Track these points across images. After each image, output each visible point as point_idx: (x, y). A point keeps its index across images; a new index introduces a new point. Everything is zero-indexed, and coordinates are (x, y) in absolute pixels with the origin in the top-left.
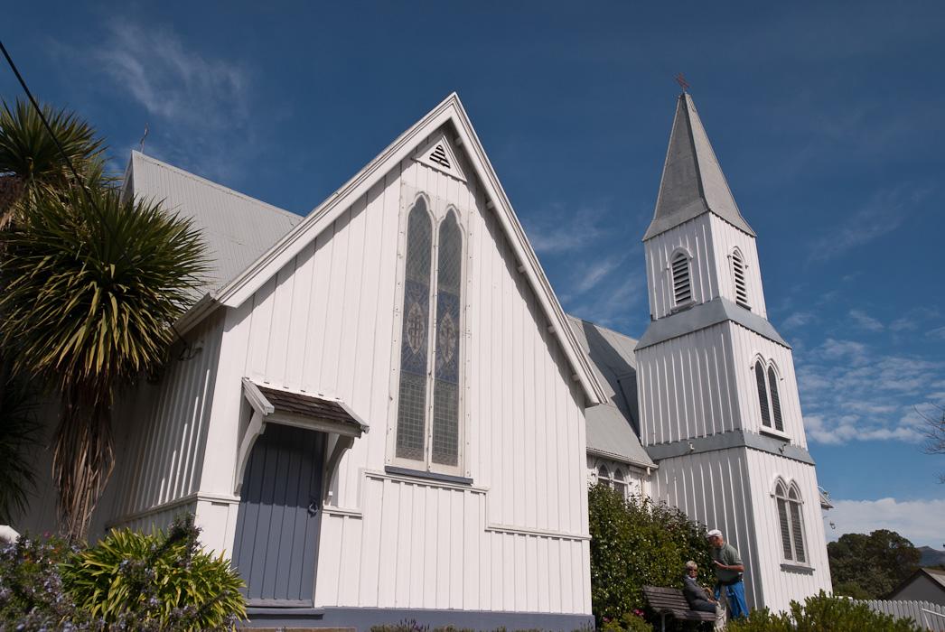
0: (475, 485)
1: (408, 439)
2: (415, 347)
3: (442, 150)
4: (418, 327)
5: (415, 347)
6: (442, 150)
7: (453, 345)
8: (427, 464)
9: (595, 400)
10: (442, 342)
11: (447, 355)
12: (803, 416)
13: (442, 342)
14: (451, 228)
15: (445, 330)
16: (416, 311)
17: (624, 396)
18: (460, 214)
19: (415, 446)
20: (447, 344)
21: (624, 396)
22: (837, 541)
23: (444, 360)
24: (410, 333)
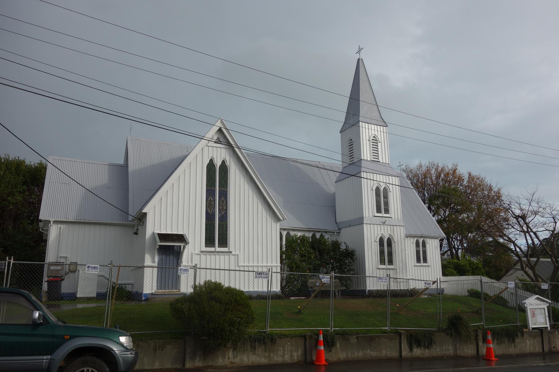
0: (233, 253)
1: (209, 241)
2: (210, 212)
3: (219, 138)
4: (211, 204)
5: (210, 212)
6: (219, 138)
7: (225, 208)
8: (422, 264)
9: (282, 219)
10: (221, 208)
11: (223, 212)
12: (47, 240)
13: (221, 208)
14: (224, 168)
15: (222, 203)
16: (211, 199)
17: (59, 239)
18: (227, 161)
19: (389, 253)
20: (223, 208)
21: (59, 239)
22: (343, 247)
23: (222, 214)
24: (208, 207)
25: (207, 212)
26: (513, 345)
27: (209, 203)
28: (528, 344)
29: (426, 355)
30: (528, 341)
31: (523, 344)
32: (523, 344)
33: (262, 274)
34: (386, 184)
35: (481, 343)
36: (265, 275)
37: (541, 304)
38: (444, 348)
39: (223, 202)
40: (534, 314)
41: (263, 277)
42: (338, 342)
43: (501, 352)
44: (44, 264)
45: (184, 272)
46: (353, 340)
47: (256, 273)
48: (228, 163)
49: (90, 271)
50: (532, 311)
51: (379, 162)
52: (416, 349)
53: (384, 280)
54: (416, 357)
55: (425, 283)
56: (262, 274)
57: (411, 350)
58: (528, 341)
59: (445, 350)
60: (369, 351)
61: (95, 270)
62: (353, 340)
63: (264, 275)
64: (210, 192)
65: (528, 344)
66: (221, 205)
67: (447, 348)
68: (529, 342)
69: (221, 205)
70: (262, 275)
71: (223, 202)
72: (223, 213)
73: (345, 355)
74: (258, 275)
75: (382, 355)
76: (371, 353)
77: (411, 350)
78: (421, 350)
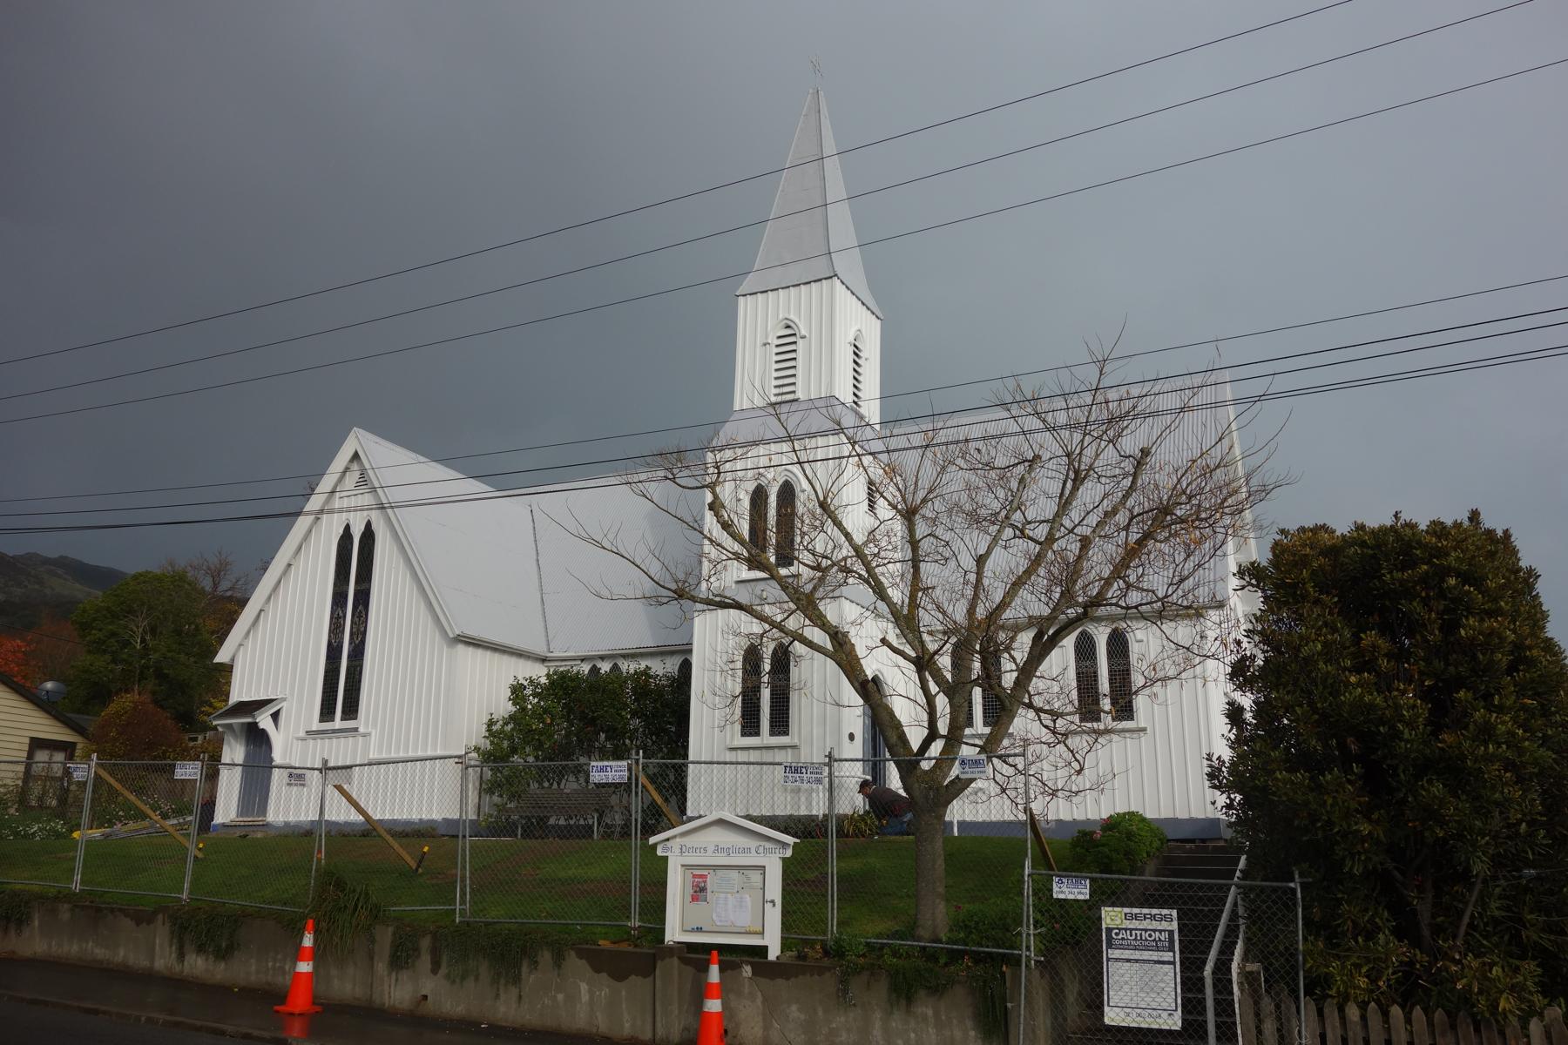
7: (362, 629)
10: (354, 630)
20: (358, 630)
24: (333, 632)
25: (330, 644)
26: (514, 991)
27: (334, 624)
28: (585, 998)
29: (219, 977)
30: (584, 987)
31: (560, 997)
32: (560, 997)
33: (804, 770)
34: (786, 470)
35: (380, 965)
36: (811, 773)
37: (746, 851)
38: (270, 964)
39: (360, 617)
40: (703, 890)
41: (805, 778)
42: (37, 915)
43: (460, 1008)
44: (686, 766)
45: (971, 770)
46: (65, 912)
47: (785, 767)
48: (374, 527)
49: (967, 773)
50: (695, 876)
51: (796, 400)
52: (194, 956)
53: (613, 773)
54: (192, 977)
55: (290, 775)
56: (804, 770)
57: (181, 956)
58: (584, 987)
59: (271, 972)
60: (90, 944)
61: (979, 769)
62: (65, 912)
63: (809, 775)
64: (339, 599)
65: (585, 998)
66: (356, 624)
67: (278, 965)
68: (591, 992)
69: (356, 624)
70: (804, 775)
71: (360, 617)
72: (357, 642)
73: (75, 948)
74: (791, 775)
75: (605, 992)
76: (97, 951)
77: (181, 956)
78: (207, 960)
